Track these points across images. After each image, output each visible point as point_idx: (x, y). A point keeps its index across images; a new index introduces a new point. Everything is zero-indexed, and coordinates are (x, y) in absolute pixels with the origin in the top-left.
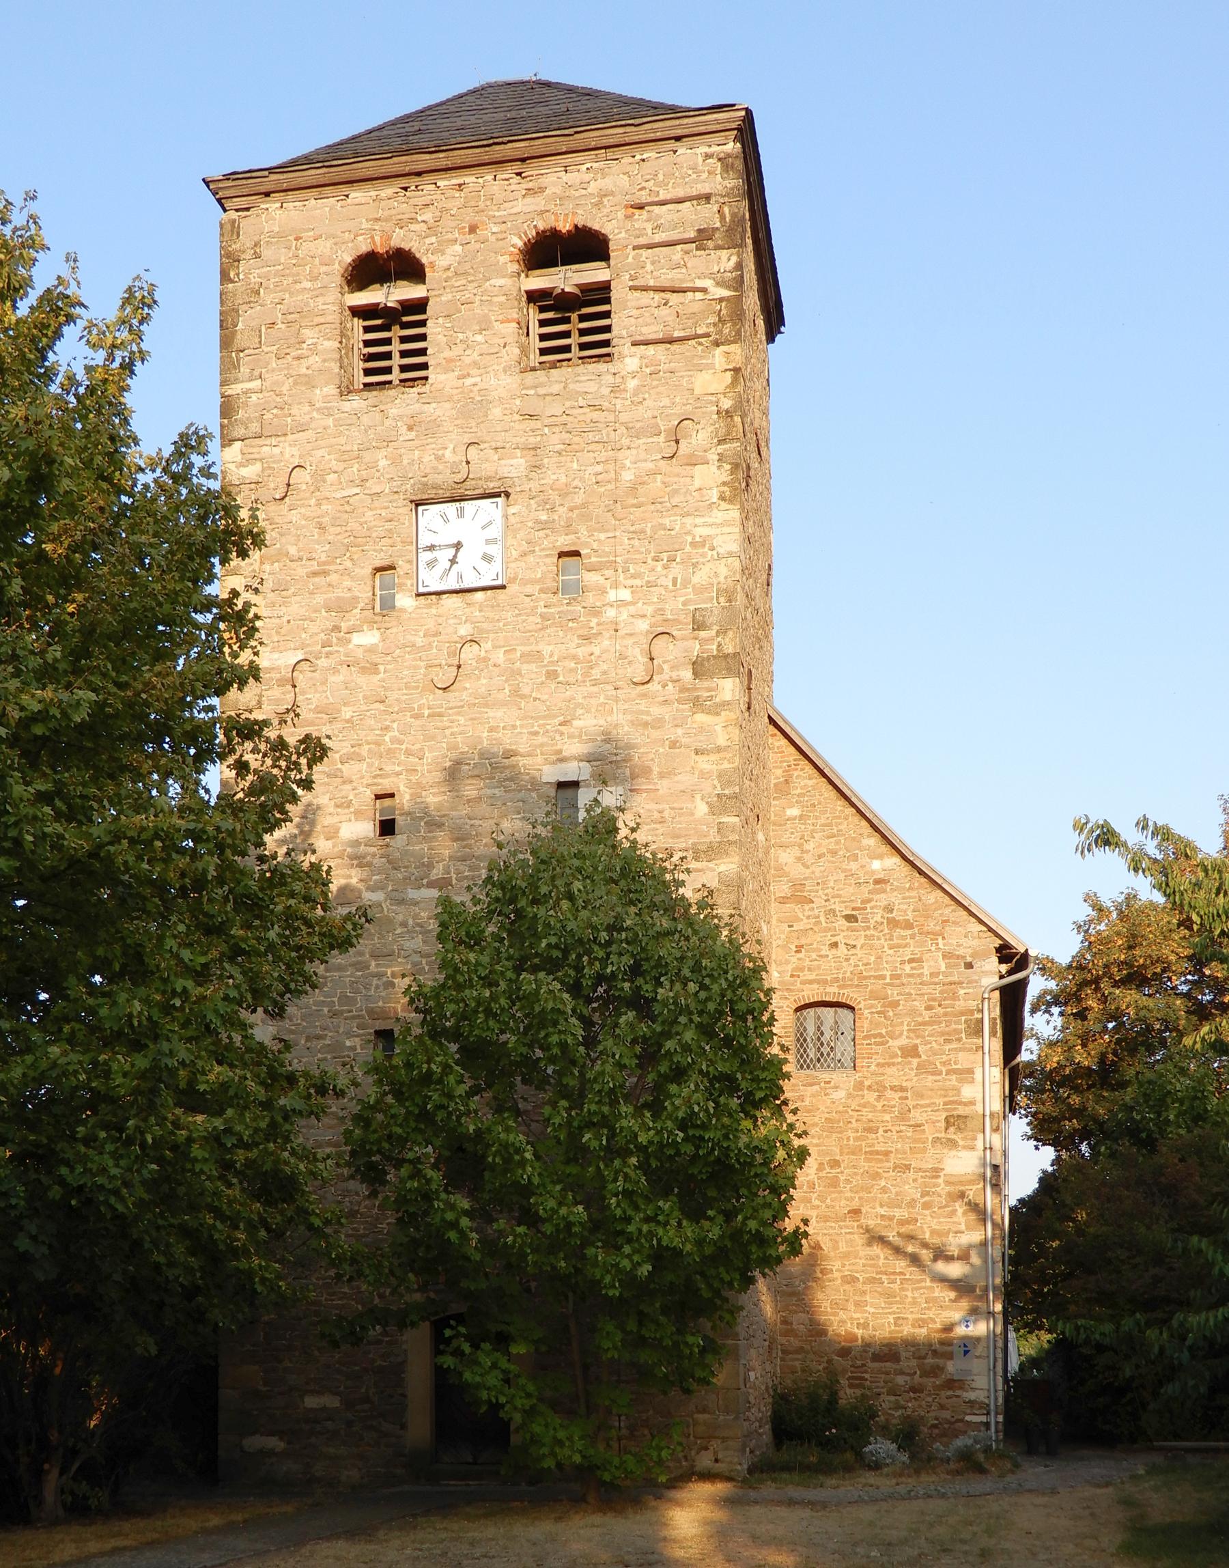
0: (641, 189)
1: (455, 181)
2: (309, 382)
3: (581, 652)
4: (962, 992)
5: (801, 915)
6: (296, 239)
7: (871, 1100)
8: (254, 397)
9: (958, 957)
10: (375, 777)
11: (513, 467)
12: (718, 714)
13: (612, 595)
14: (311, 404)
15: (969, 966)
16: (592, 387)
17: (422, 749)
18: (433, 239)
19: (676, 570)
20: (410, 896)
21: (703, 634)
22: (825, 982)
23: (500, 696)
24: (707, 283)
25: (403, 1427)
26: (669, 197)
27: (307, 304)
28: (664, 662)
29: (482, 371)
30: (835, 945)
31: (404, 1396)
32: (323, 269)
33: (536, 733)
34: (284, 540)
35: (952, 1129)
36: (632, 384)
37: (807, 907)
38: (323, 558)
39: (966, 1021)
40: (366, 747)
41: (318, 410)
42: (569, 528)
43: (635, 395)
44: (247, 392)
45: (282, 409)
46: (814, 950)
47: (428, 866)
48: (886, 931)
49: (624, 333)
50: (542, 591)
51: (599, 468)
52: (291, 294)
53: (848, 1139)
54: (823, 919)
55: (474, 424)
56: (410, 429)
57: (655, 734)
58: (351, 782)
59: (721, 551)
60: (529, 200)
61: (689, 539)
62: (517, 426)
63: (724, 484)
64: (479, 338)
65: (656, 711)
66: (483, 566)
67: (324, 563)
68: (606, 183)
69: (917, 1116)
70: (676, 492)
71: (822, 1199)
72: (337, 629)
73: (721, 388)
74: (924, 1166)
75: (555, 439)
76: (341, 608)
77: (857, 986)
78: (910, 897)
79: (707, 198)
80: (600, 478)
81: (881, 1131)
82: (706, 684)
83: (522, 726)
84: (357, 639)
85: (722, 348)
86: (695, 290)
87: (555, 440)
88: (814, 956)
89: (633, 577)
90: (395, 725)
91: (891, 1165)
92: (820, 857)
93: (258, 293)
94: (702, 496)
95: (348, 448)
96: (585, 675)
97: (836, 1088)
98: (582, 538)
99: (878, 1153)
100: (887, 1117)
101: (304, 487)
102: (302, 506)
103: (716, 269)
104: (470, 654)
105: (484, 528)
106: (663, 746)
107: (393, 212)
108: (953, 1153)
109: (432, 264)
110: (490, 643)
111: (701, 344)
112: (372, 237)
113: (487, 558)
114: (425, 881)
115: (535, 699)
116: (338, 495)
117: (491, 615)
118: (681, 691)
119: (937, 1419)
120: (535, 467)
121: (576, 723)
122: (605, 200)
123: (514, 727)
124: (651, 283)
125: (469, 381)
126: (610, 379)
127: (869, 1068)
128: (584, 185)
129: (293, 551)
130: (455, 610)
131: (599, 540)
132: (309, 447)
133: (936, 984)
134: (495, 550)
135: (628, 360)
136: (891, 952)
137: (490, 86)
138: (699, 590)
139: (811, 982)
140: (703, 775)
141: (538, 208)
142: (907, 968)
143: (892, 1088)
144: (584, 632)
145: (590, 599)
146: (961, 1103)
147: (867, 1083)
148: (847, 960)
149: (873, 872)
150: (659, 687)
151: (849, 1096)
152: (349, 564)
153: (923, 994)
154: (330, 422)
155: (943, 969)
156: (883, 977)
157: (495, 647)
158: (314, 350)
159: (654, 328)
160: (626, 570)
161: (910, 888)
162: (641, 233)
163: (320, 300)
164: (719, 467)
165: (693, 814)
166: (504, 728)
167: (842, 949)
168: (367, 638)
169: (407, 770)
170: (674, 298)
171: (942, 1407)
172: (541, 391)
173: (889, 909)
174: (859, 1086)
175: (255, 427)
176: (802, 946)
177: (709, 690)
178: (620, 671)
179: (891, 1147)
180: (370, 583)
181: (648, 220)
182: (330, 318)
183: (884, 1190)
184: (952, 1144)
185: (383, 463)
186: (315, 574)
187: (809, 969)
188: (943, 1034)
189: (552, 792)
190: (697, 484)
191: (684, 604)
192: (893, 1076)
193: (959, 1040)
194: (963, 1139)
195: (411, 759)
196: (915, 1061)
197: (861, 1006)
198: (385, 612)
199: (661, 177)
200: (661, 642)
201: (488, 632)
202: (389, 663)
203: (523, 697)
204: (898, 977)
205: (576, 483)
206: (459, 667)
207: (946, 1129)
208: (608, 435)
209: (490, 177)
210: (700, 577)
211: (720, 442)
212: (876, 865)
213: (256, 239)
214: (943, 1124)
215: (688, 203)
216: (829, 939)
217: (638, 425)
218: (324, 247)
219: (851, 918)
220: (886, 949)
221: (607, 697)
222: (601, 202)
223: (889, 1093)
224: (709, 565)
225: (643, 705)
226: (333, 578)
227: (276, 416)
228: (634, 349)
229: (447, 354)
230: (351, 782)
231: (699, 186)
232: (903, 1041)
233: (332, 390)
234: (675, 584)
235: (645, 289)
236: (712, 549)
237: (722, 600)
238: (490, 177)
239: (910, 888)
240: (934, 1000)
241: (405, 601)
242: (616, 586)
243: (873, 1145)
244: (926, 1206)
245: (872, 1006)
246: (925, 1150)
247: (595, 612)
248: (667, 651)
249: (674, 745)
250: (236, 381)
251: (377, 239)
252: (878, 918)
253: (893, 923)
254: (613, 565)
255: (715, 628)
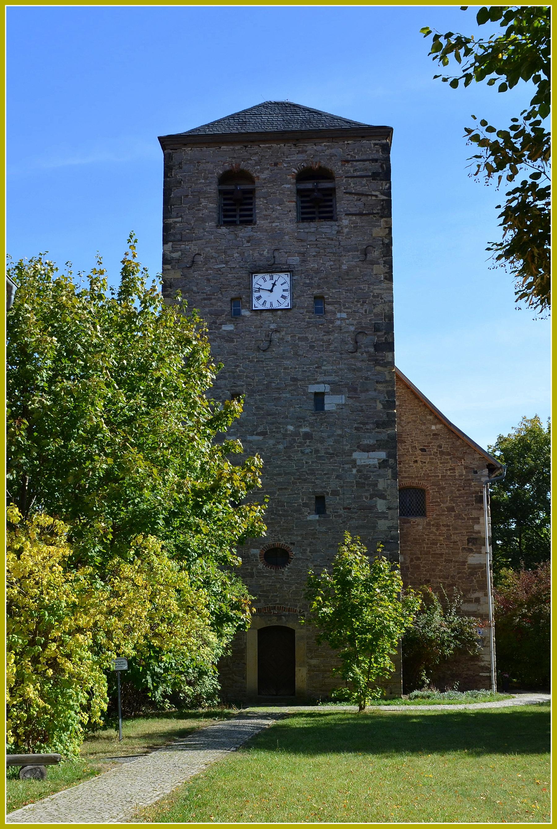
0: (348, 155)
1: (267, 145)
2: (203, 220)
3: (325, 338)
4: (473, 484)
5: (400, 448)
6: (198, 162)
7: (434, 530)
8: (178, 225)
9: (471, 468)
10: (232, 387)
11: (295, 260)
12: (386, 367)
13: (338, 315)
14: (203, 229)
15: (476, 472)
16: (329, 231)
17: (253, 376)
18: (259, 167)
19: (366, 307)
20: (248, 439)
21: (379, 333)
22: (412, 477)
23: (289, 355)
24: (377, 193)
25: (245, 678)
26: (360, 158)
27: (203, 189)
28: (362, 344)
29: (280, 221)
30: (416, 462)
31: (245, 664)
32: (210, 175)
33: (305, 371)
34: (191, 284)
35: (470, 544)
36: (346, 230)
37: (403, 445)
38: (209, 293)
39: (475, 496)
40: (228, 374)
41: (207, 232)
42: (319, 287)
43: (347, 235)
44: (176, 222)
45: (190, 230)
46: (407, 464)
47: (256, 426)
48: (439, 456)
49: (342, 210)
50: (307, 312)
51: (332, 263)
52: (196, 184)
53: (424, 548)
54: (410, 450)
55: (276, 242)
56: (248, 242)
57: (358, 374)
58: (221, 388)
59: (386, 300)
60: (300, 155)
61: (372, 294)
62: (295, 243)
63: (386, 273)
64: (278, 208)
65: (359, 364)
66: (282, 300)
67: (209, 295)
68: (333, 151)
69: (454, 538)
70: (366, 275)
71: (412, 574)
72: (215, 323)
73: (384, 235)
74: (457, 559)
75: (313, 250)
76: (218, 314)
77: (426, 480)
78: (449, 442)
79: (376, 160)
80: (332, 267)
81: (438, 545)
82: (380, 354)
83: (298, 368)
84: (224, 328)
85: (384, 219)
86: (372, 195)
87: (313, 252)
88: (407, 466)
89: (347, 308)
90: (241, 365)
91: (443, 559)
92: (408, 423)
93: (181, 183)
94: (377, 277)
95: (220, 248)
96: (328, 347)
97: (418, 525)
98: (330, 293)
99: (437, 554)
100: (441, 538)
101: (200, 263)
102: (200, 270)
103: (381, 188)
104: (275, 337)
105: (282, 285)
106: (361, 379)
107: (241, 155)
108: (472, 555)
109: (258, 177)
110: (284, 332)
111: (375, 217)
112: (232, 164)
113: (283, 297)
114: (255, 433)
115: (305, 357)
116: (216, 267)
117: (285, 321)
118: (370, 357)
119: (467, 674)
120: (304, 261)
121: (323, 368)
122: (333, 158)
123: (296, 368)
124: (353, 191)
125: (274, 225)
126: (336, 228)
127: (431, 515)
128: (323, 151)
129: (195, 289)
130: (268, 317)
131: (332, 292)
132: (203, 246)
133: (461, 480)
134: (287, 294)
135: (344, 221)
136: (441, 465)
137: (271, 103)
138: (376, 315)
139: (406, 477)
140: (380, 392)
141: (304, 159)
142: (449, 473)
143: (443, 525)
144: (326, 330)
145: (329, 316)
146: (474, 533)
147: (432, 523)
148: (422, 468)
149: (433, 430)
150: (360, 355)
151: (424, 528)
152: (220, 296)
153: (456, 484)
154: (212, 237)
155: (464, 473)
156: (438, 476)
157: (286, 334)
158: (205, 207)
159: (356, 209)
160: (344, 305)
161: (448, 438)
162: (348, 171)
163: (208, 188)
164: (384, 266)
165: (376, 408)
166: (291, 368)
167: (419, 464)
168: (229, 327)
169: (247, 384)
170: (363, 199)
171: (469, 669)
172: (307, 230)
173: (440, 446)
174: (428, 524)
175: (178, 237)
176: (401, 462)
177: (382, 356)
178: (343, 347)
179: (444, 551)
180: (230, 304)
181: (351, 167)
182: (212, 195)
183: (441, 571)
184: (471, 551)
185: (236, 255)
186: (205, 299)
187: (405, 472)
188: (465, 502)
189: (313, 397)
190: (375, 272)
191: (370, 320)
192: (444, 520)
193: (473, 505)
194: (475, 548)
195: (249, 379)
196: (453, 513)
197: (428, 489)
198: (236, 317)
199: (356, 151)
200: (360, 336)
201: (283, 327)
202: (239, 338)
203: (299, 355)
204: (445, 476)
205: (322, 268)
206: (270, 341)
207: (468, 544)
208: (336, 250)
209: (283, 145)
210: (377, 310)
211: (384, 256)
212: (433, 427)
213: (180, 161)
214: (466, 542)
215: (368, 162)
216: (414, 459)
217: (349, 247)
218: (210, 166)
219: (423, 450)
220: (439, 464)
221: (337, 358)
222: (331, 158)
223: (442, 528)
224: (381, 305)
225: (352, 361)
226: (213, 301)
227: (188, 233)
228: (346, 217)
229: (265, 213)
230: (221, 388)
231: (373, 156)
232: (448, 504)
233: (213, 224)
234: (366, 312)
235: (351, 193)
236: (382, 298)
237: (387, 320)
238: (283, 145)
239: (448, 438)
240: (461, 487)
241: (245, 313)
242: (340, 311)
243: (435, 550)
244: (459, 578)
245: (433, 489)
246: (459, 553)
247: (332, 322)
248: (364, 340)
249: (367, 379)
250: (170, 218)
251: (234, 165)
252: (435, 450)
253: (442, 453)
254: (338, 303)
255: (384, 331)
